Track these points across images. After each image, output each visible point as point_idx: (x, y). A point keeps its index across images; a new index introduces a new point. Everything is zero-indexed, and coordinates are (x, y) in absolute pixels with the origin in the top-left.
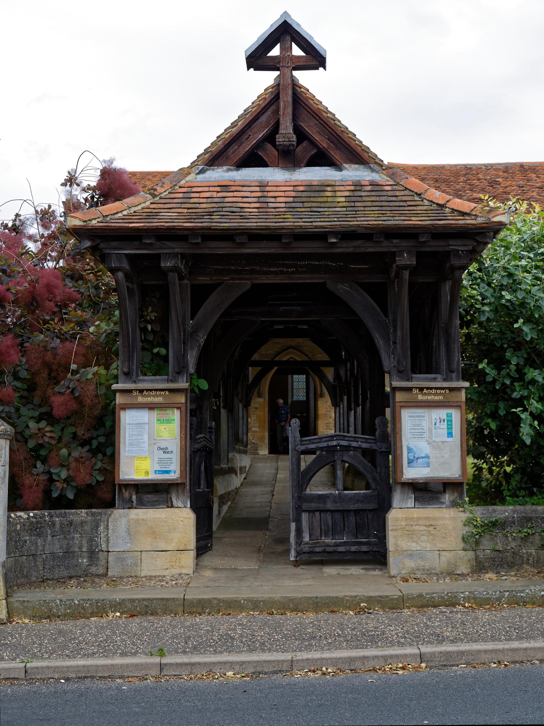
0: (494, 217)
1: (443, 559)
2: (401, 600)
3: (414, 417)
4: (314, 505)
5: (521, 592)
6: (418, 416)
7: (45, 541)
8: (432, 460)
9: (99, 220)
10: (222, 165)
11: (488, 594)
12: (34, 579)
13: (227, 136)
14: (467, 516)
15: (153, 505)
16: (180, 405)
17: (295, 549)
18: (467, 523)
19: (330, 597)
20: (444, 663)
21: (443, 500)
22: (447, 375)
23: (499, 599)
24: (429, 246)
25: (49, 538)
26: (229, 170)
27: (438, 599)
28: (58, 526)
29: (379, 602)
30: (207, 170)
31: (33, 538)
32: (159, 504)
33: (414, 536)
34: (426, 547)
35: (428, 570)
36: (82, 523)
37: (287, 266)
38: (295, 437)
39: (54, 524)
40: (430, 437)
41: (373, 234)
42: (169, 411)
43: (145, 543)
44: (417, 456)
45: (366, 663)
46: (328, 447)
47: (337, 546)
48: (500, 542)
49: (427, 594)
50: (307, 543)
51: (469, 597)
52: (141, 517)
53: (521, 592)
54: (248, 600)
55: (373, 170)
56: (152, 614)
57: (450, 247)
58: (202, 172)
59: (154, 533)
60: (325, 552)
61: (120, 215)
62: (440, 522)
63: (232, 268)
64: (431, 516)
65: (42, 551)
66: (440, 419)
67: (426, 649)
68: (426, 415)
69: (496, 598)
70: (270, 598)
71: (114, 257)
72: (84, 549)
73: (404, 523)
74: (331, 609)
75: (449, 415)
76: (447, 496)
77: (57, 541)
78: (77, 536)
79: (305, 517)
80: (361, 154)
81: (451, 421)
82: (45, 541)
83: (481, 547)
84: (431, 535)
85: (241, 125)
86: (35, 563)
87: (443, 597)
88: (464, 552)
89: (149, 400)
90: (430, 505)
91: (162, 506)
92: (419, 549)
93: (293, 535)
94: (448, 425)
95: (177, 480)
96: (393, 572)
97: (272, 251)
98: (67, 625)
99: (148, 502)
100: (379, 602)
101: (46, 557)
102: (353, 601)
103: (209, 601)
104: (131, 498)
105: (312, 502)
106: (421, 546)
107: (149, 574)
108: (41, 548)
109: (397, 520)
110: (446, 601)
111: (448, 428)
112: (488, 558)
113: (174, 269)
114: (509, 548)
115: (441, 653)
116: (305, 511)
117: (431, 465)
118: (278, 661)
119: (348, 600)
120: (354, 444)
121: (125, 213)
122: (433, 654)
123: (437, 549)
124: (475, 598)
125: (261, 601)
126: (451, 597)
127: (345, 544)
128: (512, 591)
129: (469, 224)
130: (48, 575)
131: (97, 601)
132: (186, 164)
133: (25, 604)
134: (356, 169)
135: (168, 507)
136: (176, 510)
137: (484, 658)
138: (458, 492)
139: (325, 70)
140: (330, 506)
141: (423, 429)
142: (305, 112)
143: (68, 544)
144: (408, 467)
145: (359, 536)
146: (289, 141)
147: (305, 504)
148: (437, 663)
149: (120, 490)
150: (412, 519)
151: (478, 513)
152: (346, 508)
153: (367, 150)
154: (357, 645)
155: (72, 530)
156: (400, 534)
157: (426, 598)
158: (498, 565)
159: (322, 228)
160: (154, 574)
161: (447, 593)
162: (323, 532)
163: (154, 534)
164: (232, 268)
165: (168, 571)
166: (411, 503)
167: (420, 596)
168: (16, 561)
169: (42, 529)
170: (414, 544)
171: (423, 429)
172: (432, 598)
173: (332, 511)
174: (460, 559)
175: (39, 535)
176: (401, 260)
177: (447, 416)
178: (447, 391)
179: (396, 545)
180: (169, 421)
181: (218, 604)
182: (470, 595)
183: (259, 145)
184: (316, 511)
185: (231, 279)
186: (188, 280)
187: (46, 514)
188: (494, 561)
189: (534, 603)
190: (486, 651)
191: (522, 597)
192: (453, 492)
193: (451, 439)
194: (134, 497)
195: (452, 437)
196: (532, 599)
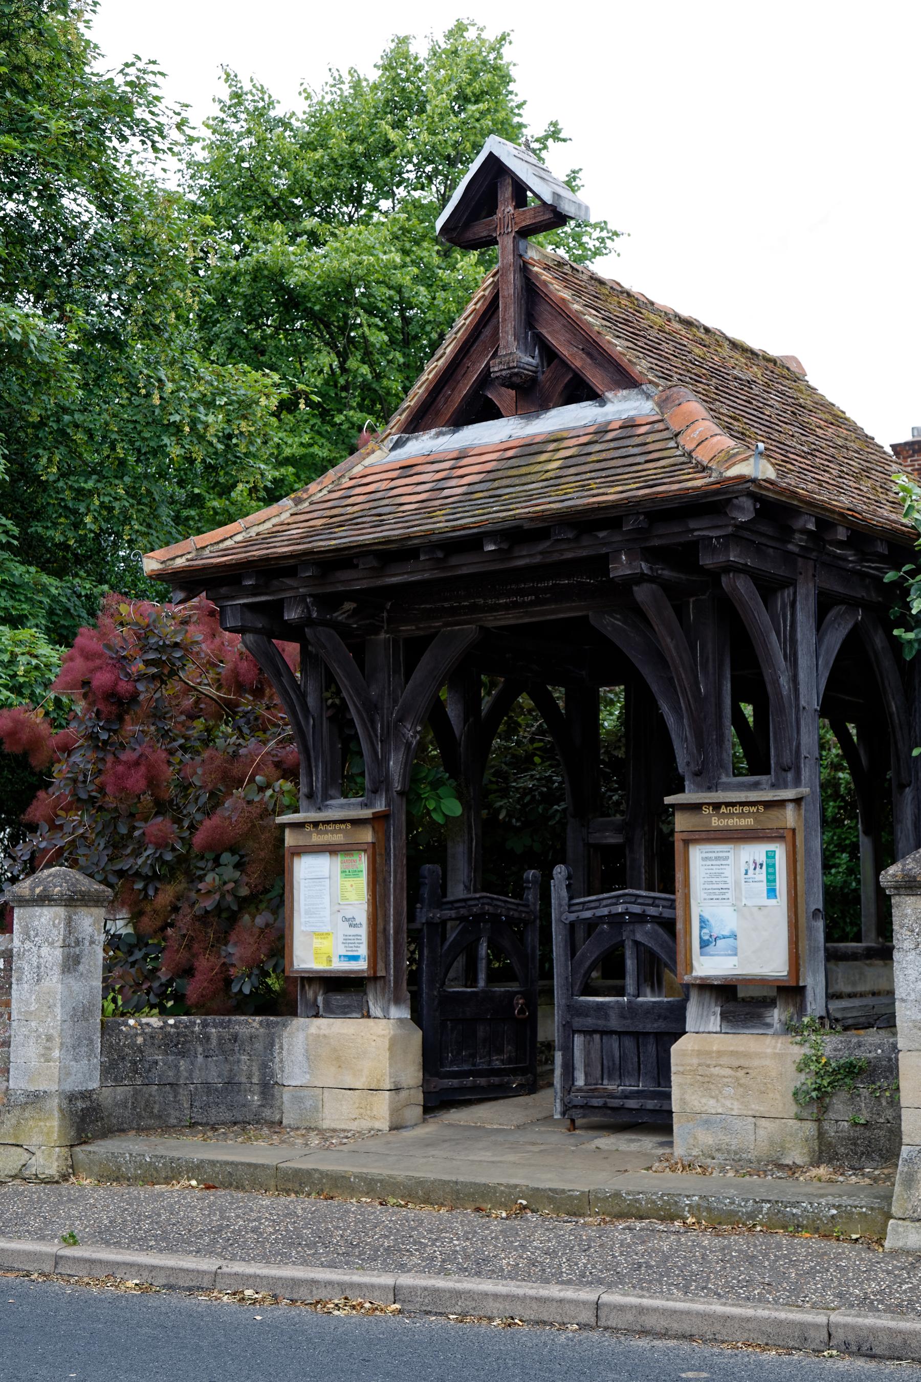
0: (728, 468)
1: (761, 1132)
2: (585, 1200)
3: (710, 859)
4: (590, 1022)
5: (796, 1204)
6: (717, 858)
7: (192, 1064)
8: (741, 942)
9: (189, 556)
10: (428, 428)
11: (732, 1203)
12: (173, 1121)
13: (431, 376)
14: (802, 1052)
15: (344, 1012)
16: (365, 847)
17: (562, 1100)
18: (802, 1066)
19: (475, 1184)
20: (429, 1309)
21: (768, 1020)
22: (777, 779)
23: (751, 1215)
24: (660, 536)
25: (200, 1059)
26: (438, 435)
27: (647, 1203)
28: (214, 1042)
29: (551, 1200)
30: (408, 439)
31: (171, 1058)
32: (352, 1012)
33: (712, 1087)
34: (732, 1109)
35: (736, 1153)
36: (251, 1038)
37: (522, 593)
38: (559, 898)
39: (208, 1038)
40: (738, 899)
41: (549, 527)
42: (356, 857)
43: (328, 1076)
44: (715, 934)
45: (315, 1292)
46: (610, 915)
47: (626, 1097)
48: (867, 1107)
49: (628, 1194)
50: (580, 1090)
51: (698, 1205)
52: (322, 1032)
53: (796, 1204)
54: (360, 1177)
56: (237, 1188)
57: (696, 533)
59: (338, 1058)
60: (605, 1106)
61: (229, 543)
62: (756, 1063)
63: (446, 605)
64: (741, 1049)
65: (187, 1078)
66: (755, 863)
67: (406, 1280)
68: (731, 855)
69: (747, 1213)
70: (390, 1177)
71: (229, 610)
72: (255, 1080)
73: (695, 1061)
74: (478, 1205)
75: (770, 855)
76: (776, 1012)
77: (213, 1065)
78: (244, 1058)
79: (578, 1040)
80: (627, 368)
81: (774, 866)
82: (192, 1064)
83: (831, 1115)
84: (740, 1085)
85: (452, 351)
86: (175, 1097)
87: (654, 1202)
88: (799, 1123)
89: (732, 822)
90: (747, 1028)
91: (354, 1015)
92: (720, 1111)
93: (558, 1072)
94: (768, 874)
95: (363, 971)
96: (679, 1150)
97: (427, 575)
99: (338, 1007)
100: (551, 1200)
101: (196, 1089)
102: (511, 1194)
103: (309, 1173)
104: (316, 999)
105: (587, 1016)
106: (723, 1106)
107: (334, 1125)
108: (185, 1074)
109: (684, 1053)
110: (660, 1209)
111: (768, 881)
112: (843, 1138)
114: (882, 1120)
115: (425, 1289)
116: (579, 1032)
117: (739, 951)
118: (198, 1271)
119: (502, 1192)
120: (652, 911)
121: (239, 538)
122: (413, 1289)
123: (750, 1113)
124: (709, 1209)
125: (379, 1181)
126: (667, 1202)
127: (638, 1094)
128: (777, 1202)
129: (688, 489)
130: (198, 1118)
131: (172, 1160)
133: (91, 1156)
134: (625, 399)
135: (363, 1017)
136: (370, 1022)
137: (492, 1307)
138: (795, 1005)
140: (614, 1023)
141: (725, 883)
142: (548, 308)
143: (231, 1070)
144: (702, 954)
145: (662, 1082)
146: (509, 368)
147: (577, 1019)
148: (417, 1306)
149: (303, 987)
150: (708, 1053)
151: (829, 1047)
152: (640, 1028)
154: (333, 1260)
155: (237, 1049)
156: (688, 1081)
157: (625, 1200)
158: (863, 1154)
159: (464, 529)
160: (339, 1127)
161: (663, 1195)
162: (606, 1071)
163: (339, 1060)
164: (446, 605)
165: (356, 1123)
166: (714, 1023)
167: (617, 1195)
168: (136, 1093)
169: (188, 1045)
170: (712, 1102)
171: (725, 883)
172: (637, 1201)
173: (619, 1034)
174: (791, 1135)
175: (182, 1054)
176: (616, 568)
177: (767, 857)
178: (761, 808)
179: (683, 1101)
180: (356, 874)
181: (320, 1179)
182: (700, 1202)
184: (595, 1032)
185: (447, 624)
186: (387, 632)
187: (198, 1021)
188: (855, 1144)
189: (817, 1230)
190: (496, 1296)
191: (794, 1215)
192: (787, 1004)
193: (773, 902)
194: (320, 999)
195: (776, 897)
196: (814, 1221)
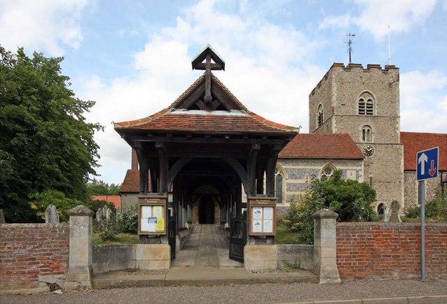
1: (266, 264)
55: (243, 112)
58: (173, 111)
98: (115, 291)
113: (161, 148)
132: (167, 107)
139: (94, 103)
153: (240, 104)
183: (197, 100)
